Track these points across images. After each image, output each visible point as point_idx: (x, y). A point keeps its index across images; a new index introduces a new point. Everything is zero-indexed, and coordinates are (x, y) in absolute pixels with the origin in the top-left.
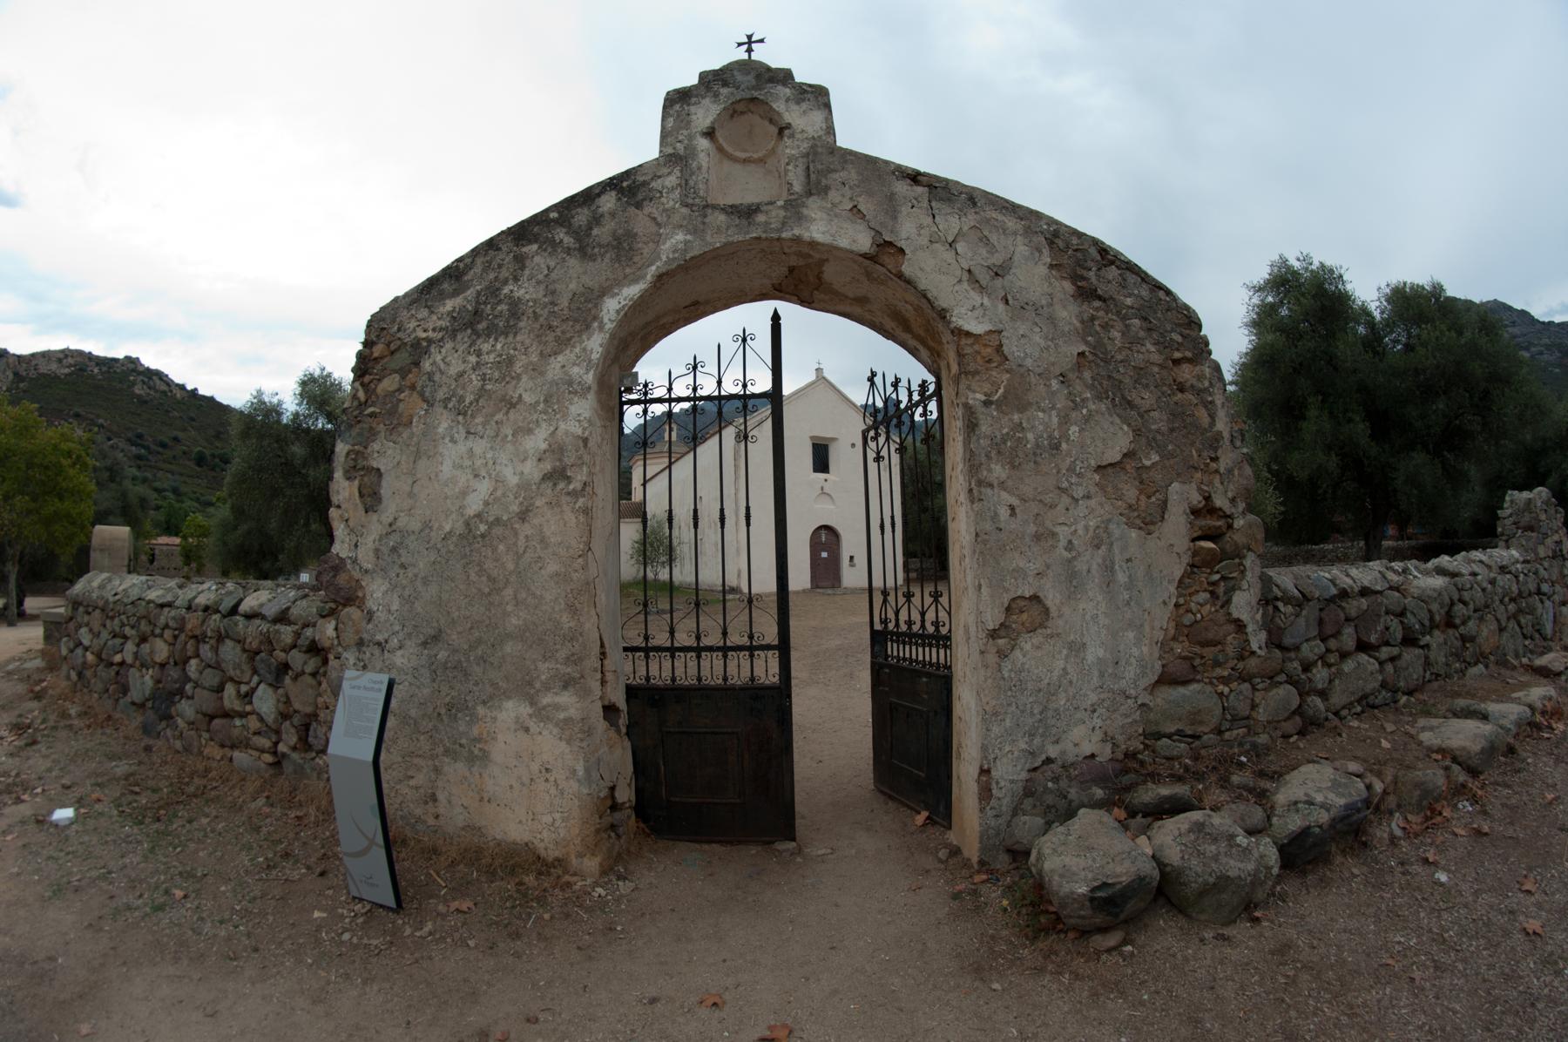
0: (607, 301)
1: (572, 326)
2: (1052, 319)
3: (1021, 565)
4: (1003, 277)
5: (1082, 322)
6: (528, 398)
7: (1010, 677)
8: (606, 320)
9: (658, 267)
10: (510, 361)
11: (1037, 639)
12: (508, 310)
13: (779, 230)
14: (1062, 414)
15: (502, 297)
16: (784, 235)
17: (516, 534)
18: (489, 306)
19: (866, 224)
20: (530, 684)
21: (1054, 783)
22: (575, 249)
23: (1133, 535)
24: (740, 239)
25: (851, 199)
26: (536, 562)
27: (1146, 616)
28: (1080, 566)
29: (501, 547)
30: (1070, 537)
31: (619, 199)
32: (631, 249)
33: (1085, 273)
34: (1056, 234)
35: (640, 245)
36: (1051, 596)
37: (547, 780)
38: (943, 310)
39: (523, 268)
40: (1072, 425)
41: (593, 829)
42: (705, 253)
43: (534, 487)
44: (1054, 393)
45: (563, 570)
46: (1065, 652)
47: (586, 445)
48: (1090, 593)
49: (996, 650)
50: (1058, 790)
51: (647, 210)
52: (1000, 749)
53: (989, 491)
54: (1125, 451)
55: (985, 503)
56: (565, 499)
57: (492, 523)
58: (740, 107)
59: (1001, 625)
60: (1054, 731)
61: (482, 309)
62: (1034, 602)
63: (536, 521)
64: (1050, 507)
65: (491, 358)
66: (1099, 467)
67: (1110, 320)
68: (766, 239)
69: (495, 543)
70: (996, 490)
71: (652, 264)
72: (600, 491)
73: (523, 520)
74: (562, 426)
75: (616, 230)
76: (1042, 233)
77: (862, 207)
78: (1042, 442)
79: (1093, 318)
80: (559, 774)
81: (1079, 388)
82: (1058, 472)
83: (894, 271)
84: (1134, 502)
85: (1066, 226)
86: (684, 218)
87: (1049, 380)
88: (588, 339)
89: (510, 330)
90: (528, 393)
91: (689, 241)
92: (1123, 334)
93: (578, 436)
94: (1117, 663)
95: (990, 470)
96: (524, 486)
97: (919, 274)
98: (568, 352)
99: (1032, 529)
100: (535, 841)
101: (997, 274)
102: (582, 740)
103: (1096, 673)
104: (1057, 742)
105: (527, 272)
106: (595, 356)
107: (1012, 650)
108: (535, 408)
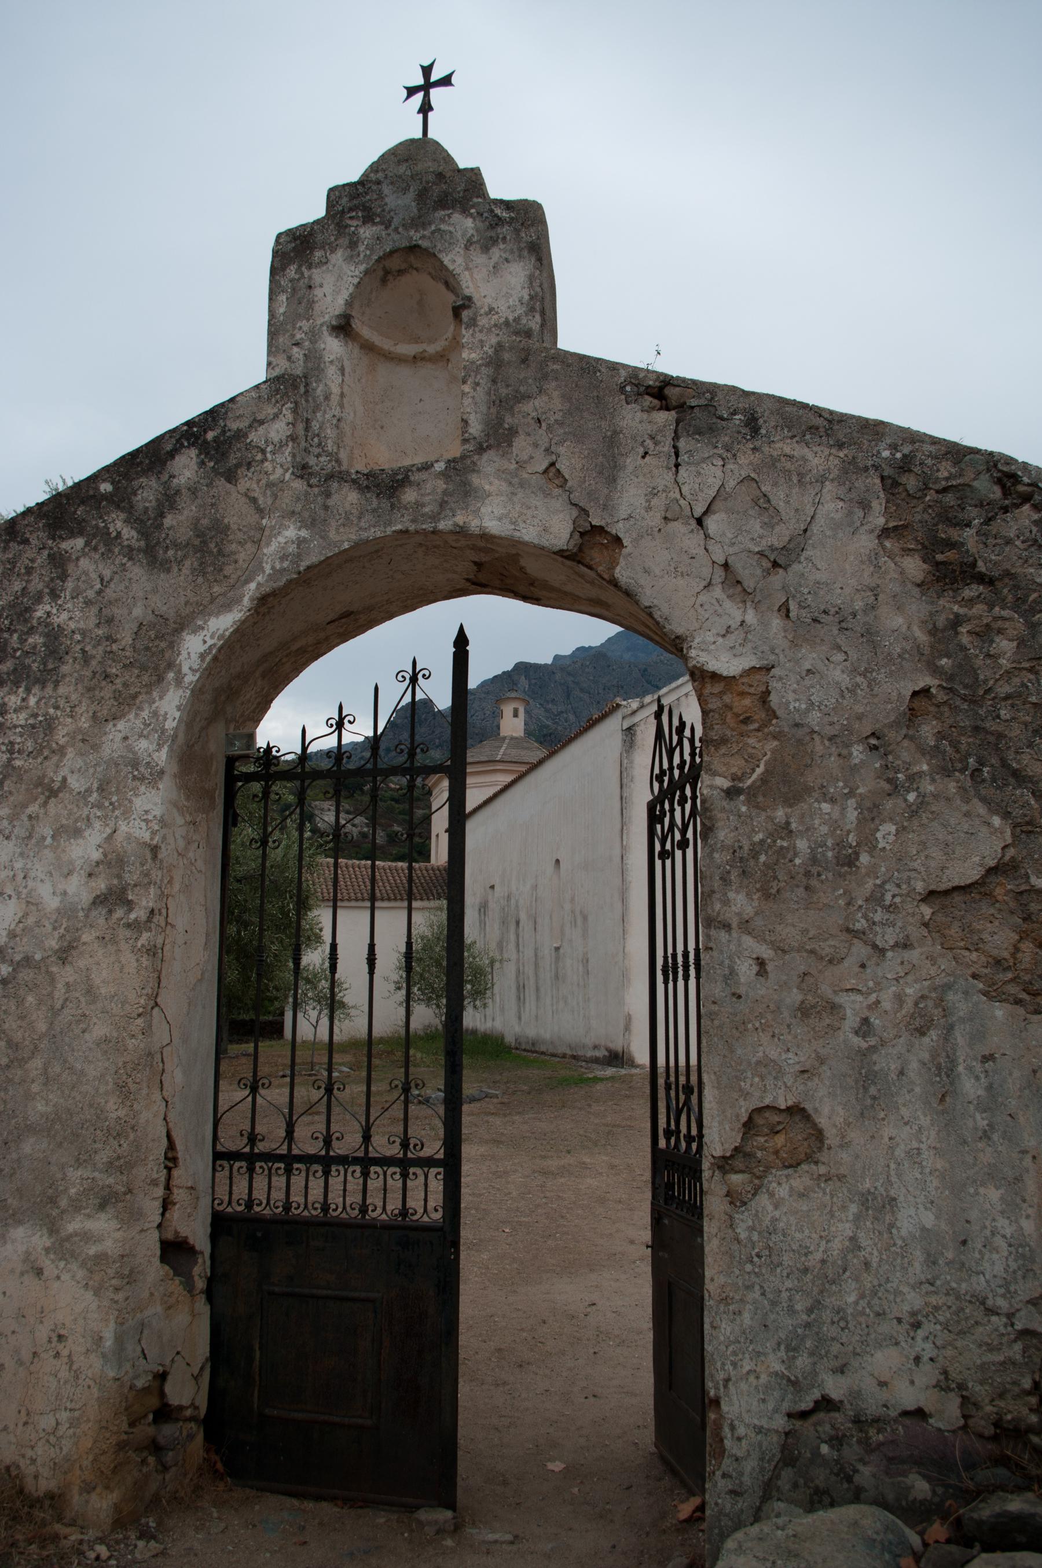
0: (188, 638)
1: (138, 676)
2: (869, 635)
3: (773, 1054)
4: (785, 569)
5: (933, 632)
6: (75, 783)
7: (750, 1239)
8: (185, 669)
9: (259, 584)
10: (50, 726)
11: (800, 1180)
12: (45, 645)
13: (435, 517)
14: (868, 804)
15: (35, 622)
16: (442, 525)
17: (53, 980)
18: (15, 636)
19: (565, 497)
20: (53, 1201)
21: (832, 1447)
22: (139, 550)
23: (999, 1013)
24: (379, 534)
25: (548, 450)
26: (79, 1022)
27: (1028, 1161)
28: (886, 1062)
29: (30, 999)
30: (866, 1013)
31: (202, 464)
32: (220, 553)
33: (954, 534)
34: (905, 465)
35: (233, 547)
36: (826, 1110)
37: (57, 1355)
38: (677, 637)
39: (64, 577)
40: (883, 821)
41: (114, 1440)
42: (328, 558)
43: (81, 914)
44: (854, 769)
45: (115, 1034)
46: (853, 1208)
47: (155, 857)
48: (905, 1112)
49: (724, 1191)
50: (837, 1462)
51: (244, 484)
52: (734, 1364)
53: (723, 935)
54: (992, 863)
55: (715, 954)
56: (123, 933)
57: (18, 963)
58: (395, 263)
59: (736, 1149)
60: (835, 1348)
61: (6, 640)
62: (797, 1118)
63: (82, 963)
64: (830, 961)
65: (21, 718)
66: (932, 893)
67: (996, 619)
68: (417, 532)
69: (21, 992)
70: (734, 934)
71: (247, 581)
72: (181, 921)
73: (64, 961)
74: (123, 828)
75: (198, 520)
76: (876, 467)
77: (563, 466)
78: (824, 855)
79: (957, 622)
80: (76, 1345)
81: (905, 756)
82: (848, 904)
83: (606, 576)
84: (1006, 954)
85: (935, 441)
86: (298, 499)
87: (848, 746)
88: (161, 698)
89: (47, 677)
90: (76, 776)
91: (305, 540)
92: (1021, 643)
93: (145, 843)
94: (964, 1242)
95: (726, 902)
96: (67, 912)
97: (644, 580)
98: (132, 716)
99: (795, 996)
100: (22, 1463)
101: (775, 564)
102: (117, 1289)
103: (919, 1255)
104: (841, 1370)
105: (70, 584)
106: (170, 724)
107: (754, 1195)
108: (85, 799)
